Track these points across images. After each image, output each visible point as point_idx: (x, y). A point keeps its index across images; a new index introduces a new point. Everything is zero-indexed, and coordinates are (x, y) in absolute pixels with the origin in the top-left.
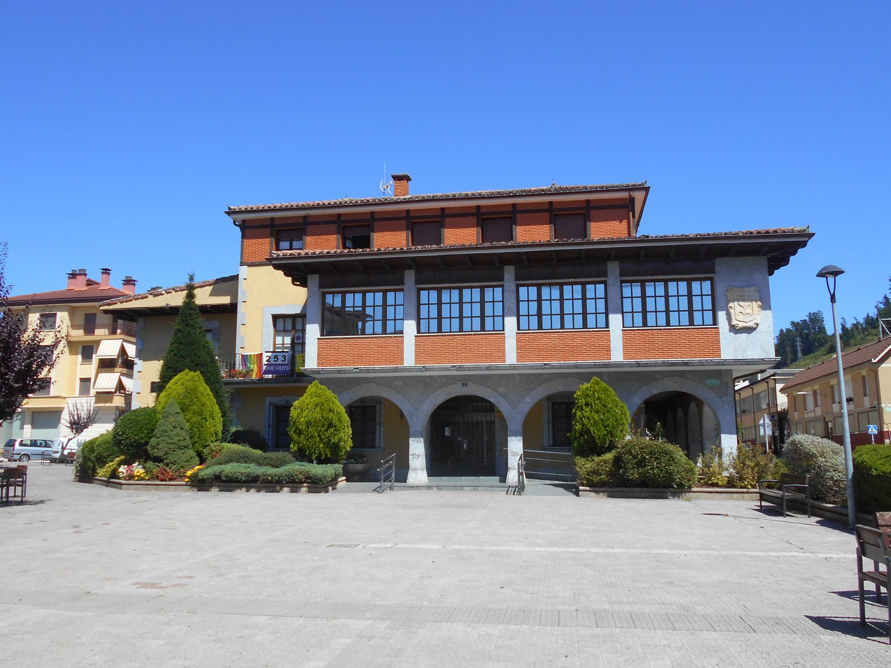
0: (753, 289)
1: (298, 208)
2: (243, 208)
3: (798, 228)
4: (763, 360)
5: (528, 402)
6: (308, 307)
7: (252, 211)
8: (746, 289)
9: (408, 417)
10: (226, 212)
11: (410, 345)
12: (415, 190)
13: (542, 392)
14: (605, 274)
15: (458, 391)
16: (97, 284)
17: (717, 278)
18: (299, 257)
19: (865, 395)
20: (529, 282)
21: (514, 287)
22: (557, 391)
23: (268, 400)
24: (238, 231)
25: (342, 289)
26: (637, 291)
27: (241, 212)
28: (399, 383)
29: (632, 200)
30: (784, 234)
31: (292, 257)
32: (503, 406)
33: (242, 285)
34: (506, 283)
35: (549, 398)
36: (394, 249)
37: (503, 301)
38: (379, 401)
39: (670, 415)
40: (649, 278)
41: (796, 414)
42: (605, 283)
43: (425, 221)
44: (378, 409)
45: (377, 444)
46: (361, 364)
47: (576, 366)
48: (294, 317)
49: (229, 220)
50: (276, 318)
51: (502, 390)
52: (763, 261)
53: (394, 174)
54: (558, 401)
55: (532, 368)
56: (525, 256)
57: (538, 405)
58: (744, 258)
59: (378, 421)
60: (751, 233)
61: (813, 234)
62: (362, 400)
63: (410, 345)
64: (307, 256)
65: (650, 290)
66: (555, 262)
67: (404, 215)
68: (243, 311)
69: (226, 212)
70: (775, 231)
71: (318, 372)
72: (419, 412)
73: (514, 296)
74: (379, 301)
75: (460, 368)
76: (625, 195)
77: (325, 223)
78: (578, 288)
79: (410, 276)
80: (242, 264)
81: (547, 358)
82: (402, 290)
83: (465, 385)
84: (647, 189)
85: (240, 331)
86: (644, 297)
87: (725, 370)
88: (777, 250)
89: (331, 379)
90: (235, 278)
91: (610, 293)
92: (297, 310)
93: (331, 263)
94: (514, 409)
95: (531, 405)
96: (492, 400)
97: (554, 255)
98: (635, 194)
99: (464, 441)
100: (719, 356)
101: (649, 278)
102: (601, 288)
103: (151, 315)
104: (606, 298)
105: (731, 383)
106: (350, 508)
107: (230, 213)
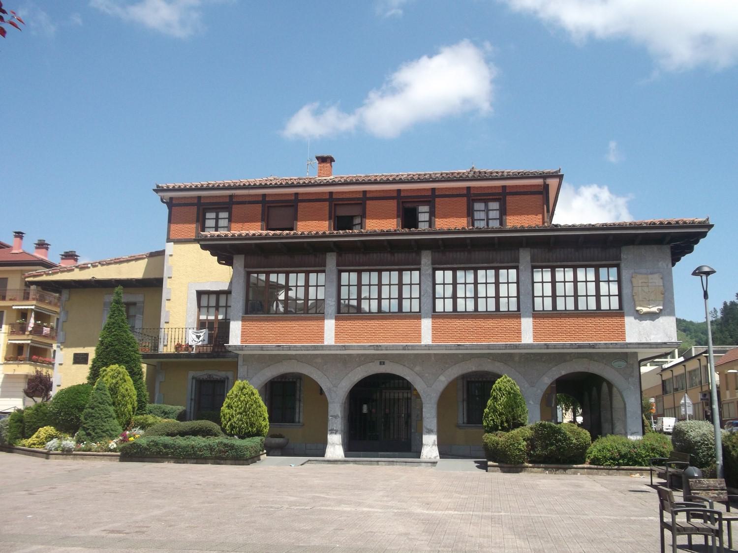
0: (656, 276)
1: (224, 188)
2: (171, 186)
3: (701, 219)
4: (665, 343)
5: (443, 381)
6: (234, 285)
7: (180, 189)
8: (650, 276)
9: (327, 394)
10: (154, 190)
11: (334, 330)
12: (337, 172)
13: (455, 372)
14: (517, 261)
15: (375, 369)
16: (8, 247)
17: (622, 265)
18: (226, 238)
19: (727, 389)
20: (445, 266)
21: (430, 271)
22: (470, 370)
23: (191, 374)
24: (165, 209)
25: (266, 269)
26: (547, 276)
27: (168, 190)
28: (319, 360)
29: (546, 187)
30: (685, 225)
31: (219, 238)
32: (419, 385)
33: (168, 262)
34: (423, 268)
35: (464, 377)
36: (317, 233)
37: (420, 298)
38: (300, 377)
39: (595, 389)
40: (559, 264)
41: (728, 392)
42: (517, 268)
43: (346, 206)
44: (298, 385)
45: (297, 420)
46: (283, 342)
47: (489, 347)
48: (218, 293)
49: (157, 197)
50: (200, 294)
51: (417, 368)
52: (667, 251)
53: (320, 155)
54: (473, 379)
55: (447, 347)
56: (440, 242)
57: (452, 385)
58: (648, 247)
59: (298, 397)
60: (654, 223)
61: (712, 226)
62: (283, 376)
63: (334, 330)
64: (233, 238)
65: (559, 276)
66: (469, 248)
67: (328, 197)
68: (168, 286)
69: (154, 190)
70: (677, 222)
71: (241, 348)
72: (337, 391)
73: (430, 279)
74: (301, 282)
75: (378, 347)
76: (540, 181)
77: (250, 203)
78: (302, 276)
79: (331, 260)
80: (169, 240)
81: (460, 339)
82: (324, 271)
83: (382, 363)
84: (561, 177)
85: (166, 306)
86: (554, 282)
87: (631, 353)
88: (679, 240)
89: (254, 355)
90: (161, 253)
91: (522, 278)
92: (225, 287)
93: (256, 244)
94: (429, 390)
95: (446, 383)
96: (408, 378)
97: (468, 241)
98: (550, 181)
99: (380, 420)
100: (624, 339)
101: (559, 264)
102: (513, 273)
103: (75, 287)
104: (518, 283)
105: (636, 365)
106: (276, 479)
107: (159, 190)
